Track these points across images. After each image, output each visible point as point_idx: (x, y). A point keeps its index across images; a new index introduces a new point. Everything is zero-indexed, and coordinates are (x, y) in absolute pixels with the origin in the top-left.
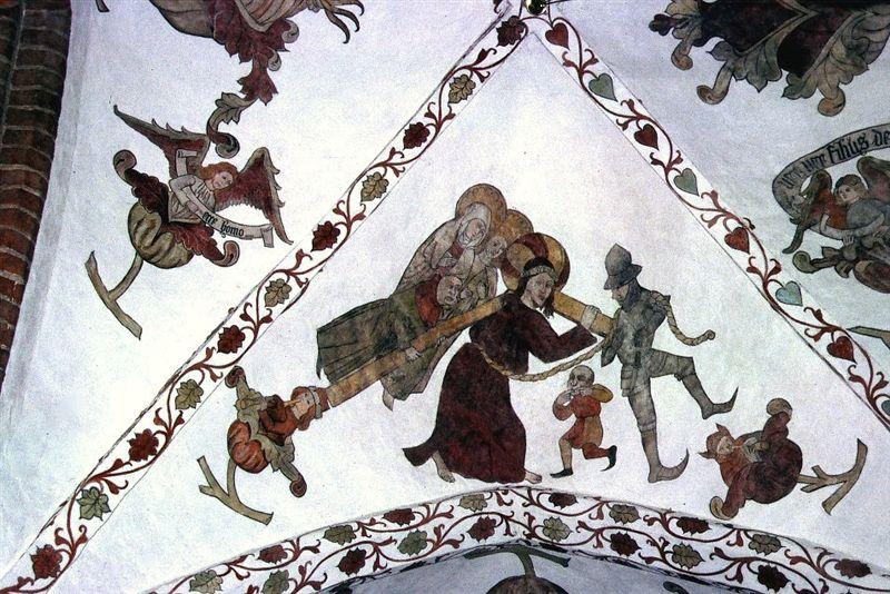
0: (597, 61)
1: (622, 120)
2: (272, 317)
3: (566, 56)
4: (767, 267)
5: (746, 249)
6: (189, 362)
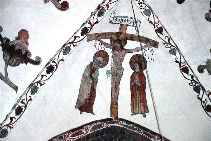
0: (11, 129)
1: (164, 42)
2: (98, 21)
3: (199, 96)
4: (90, 127)
5: (175, 55)
6: (67, 42)
